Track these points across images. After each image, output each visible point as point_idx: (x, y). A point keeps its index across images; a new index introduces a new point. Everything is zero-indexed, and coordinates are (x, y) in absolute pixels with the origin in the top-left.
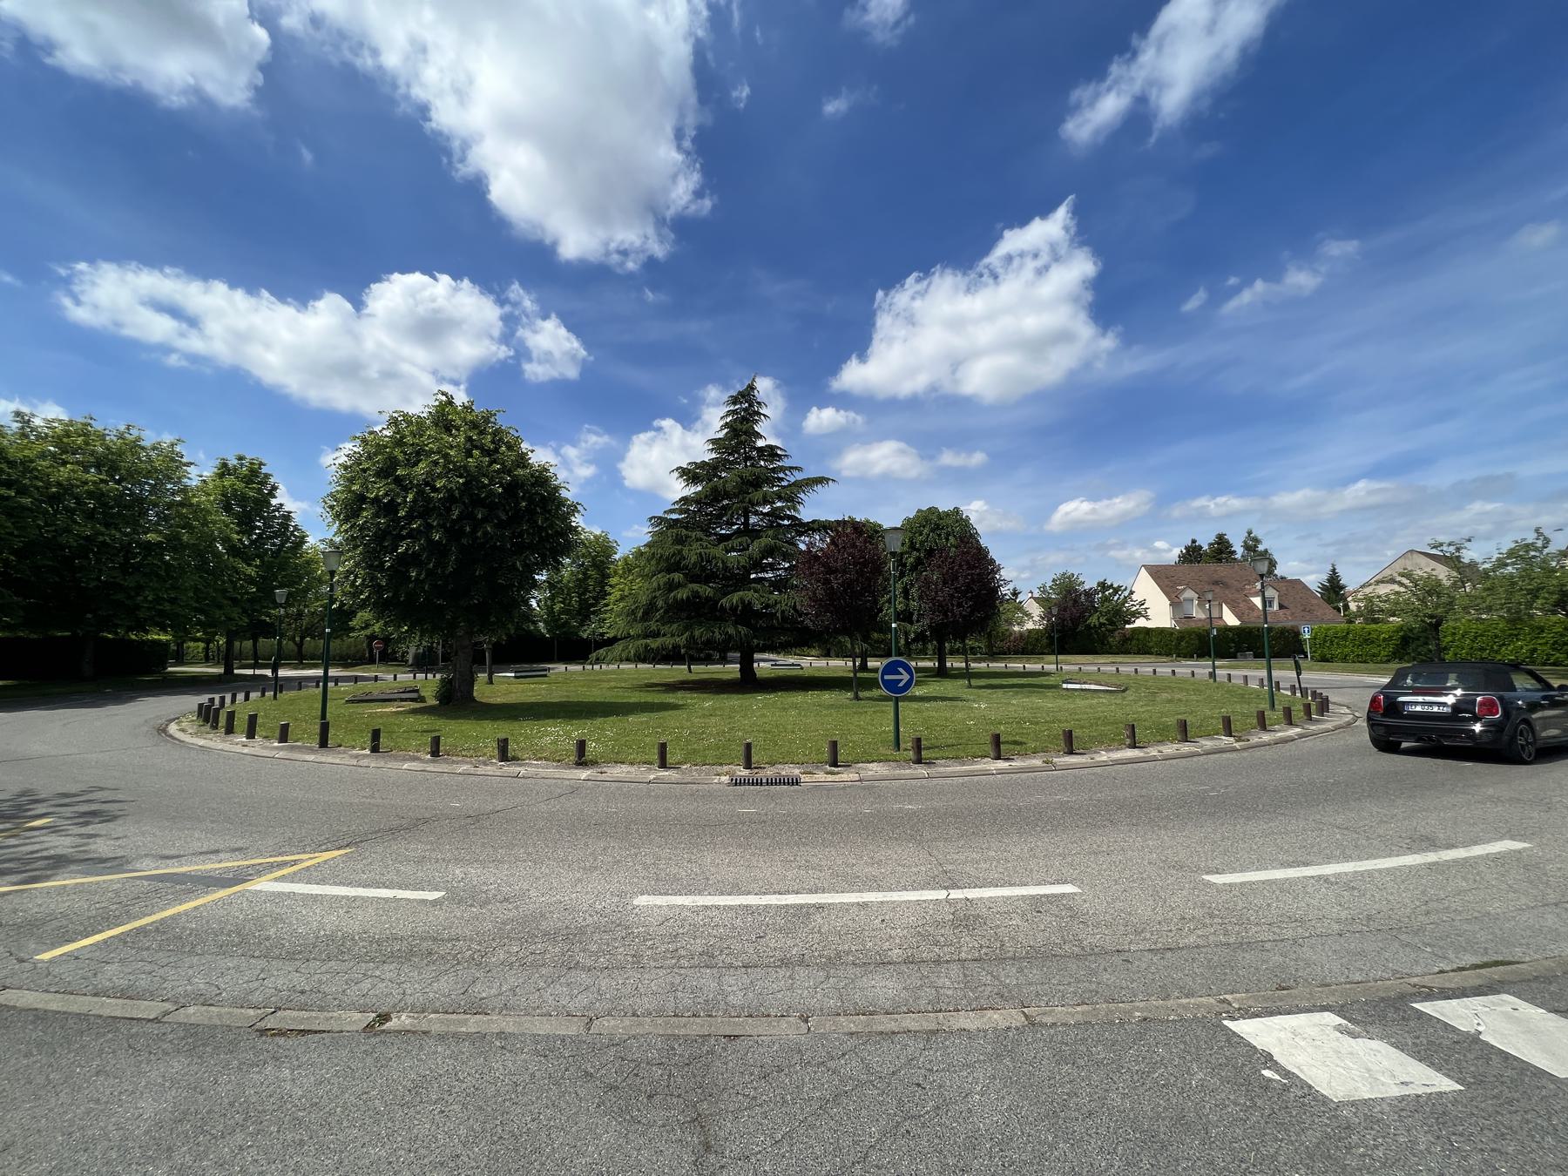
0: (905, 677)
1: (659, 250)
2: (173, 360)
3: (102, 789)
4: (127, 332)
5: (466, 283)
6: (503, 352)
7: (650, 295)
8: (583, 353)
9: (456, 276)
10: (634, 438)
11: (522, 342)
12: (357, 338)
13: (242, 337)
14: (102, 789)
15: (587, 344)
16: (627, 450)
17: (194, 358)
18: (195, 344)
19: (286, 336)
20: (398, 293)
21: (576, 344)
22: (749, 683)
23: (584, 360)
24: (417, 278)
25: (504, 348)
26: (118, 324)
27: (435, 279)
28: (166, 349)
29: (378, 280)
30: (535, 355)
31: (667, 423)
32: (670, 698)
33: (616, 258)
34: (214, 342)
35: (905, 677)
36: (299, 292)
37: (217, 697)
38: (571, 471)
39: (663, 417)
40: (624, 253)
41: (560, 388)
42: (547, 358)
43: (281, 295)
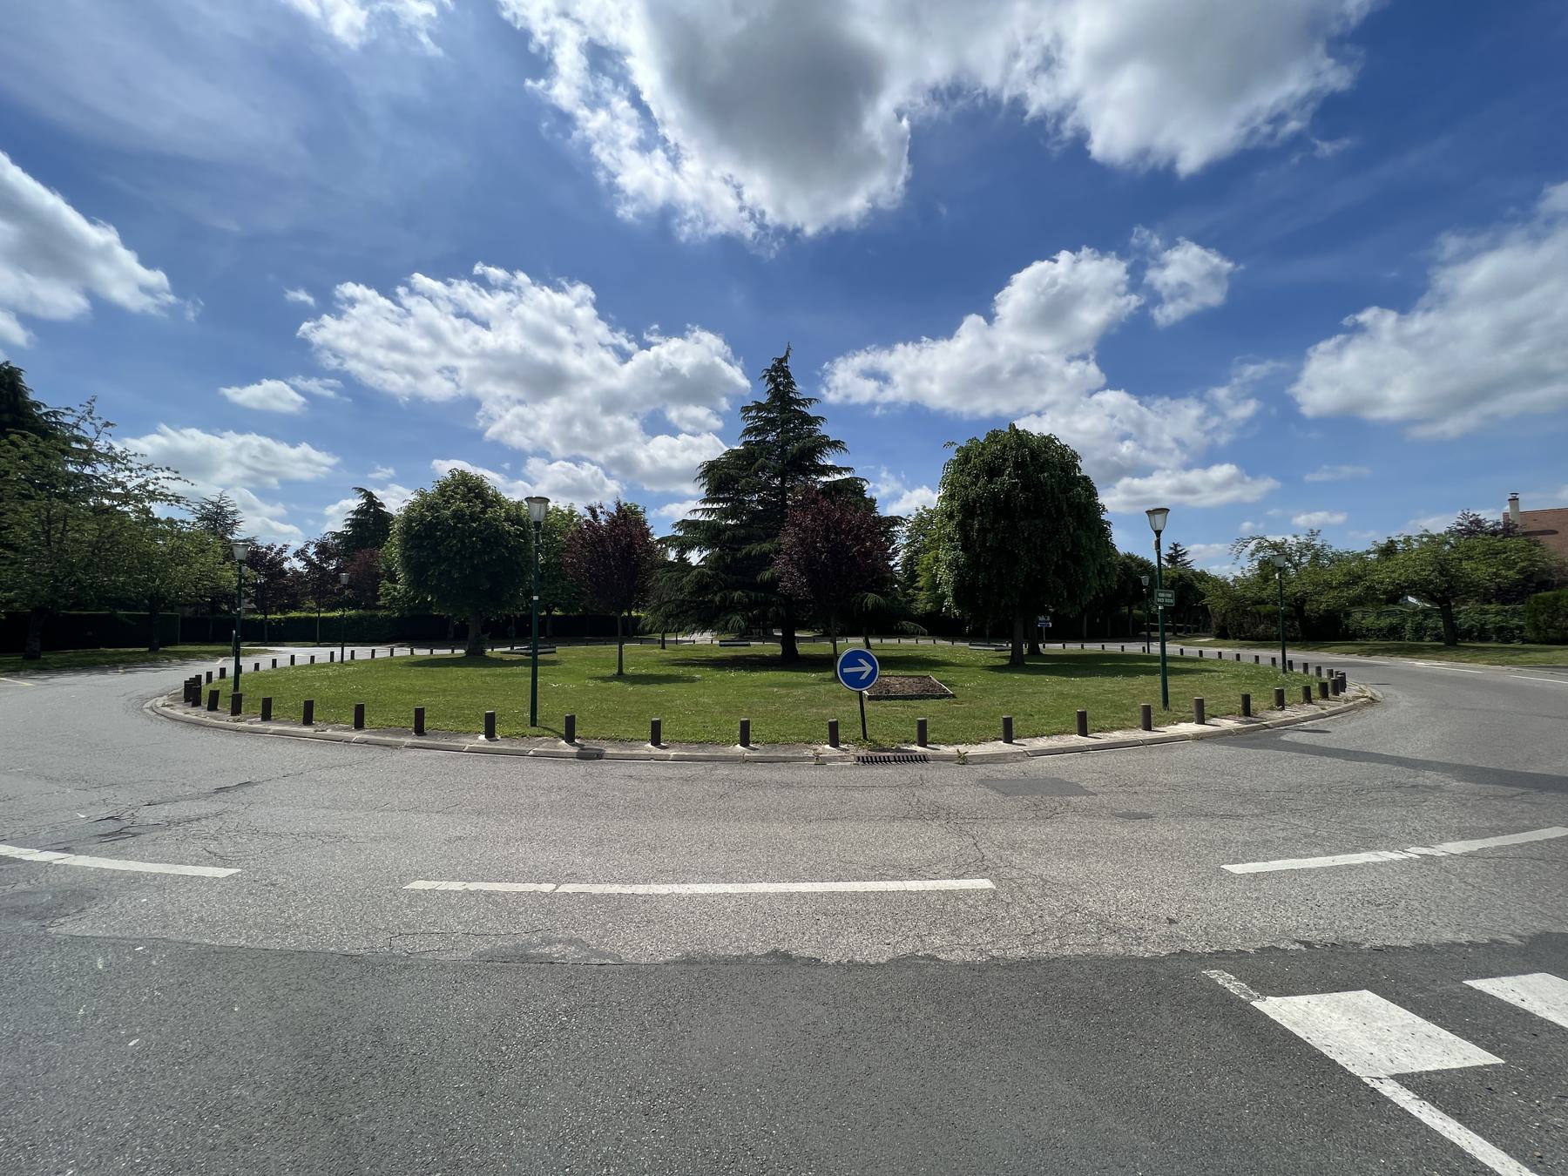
0: (868, 668)
1: (1338, 78)
2: (877, 412)
3: (1504, 798)
4: (853, 401)
5: (1085, 251)
6: (1134, 300)
7: (1326, 148)
8: (1228, 265)
9: (1074, 249)
10: (1310, 351)
11: (1150, 286)
12: (991, 346)
13: (913, 378)
14: (1504, 798)
15: (1225, 252)
16: (1300, 369)
17: (889, 406)
18: (889, 395)
19: (942, 367)
20: (1023, 289)
21: (1215, 260)
22: (790, 660)
23: (1230, 275)
24: (1038, 267)
25: (1134, 298)
26: (848, 397)
27: (1056, 261)
28: (873, 404)
29: (1000, 288)
30: (1165, 294)
31: (1367, 316)
32: (680, 671)
33: (1267, 129)
34: (899, 391)
35: (868, 668)
36: (945, 329)
37: (337, 651)
38: (1224, 415)
39: (1360, 308)
40: (1278, 119)
41: (1204, 324)
42: (1183, 290)
43: (934, 337)
